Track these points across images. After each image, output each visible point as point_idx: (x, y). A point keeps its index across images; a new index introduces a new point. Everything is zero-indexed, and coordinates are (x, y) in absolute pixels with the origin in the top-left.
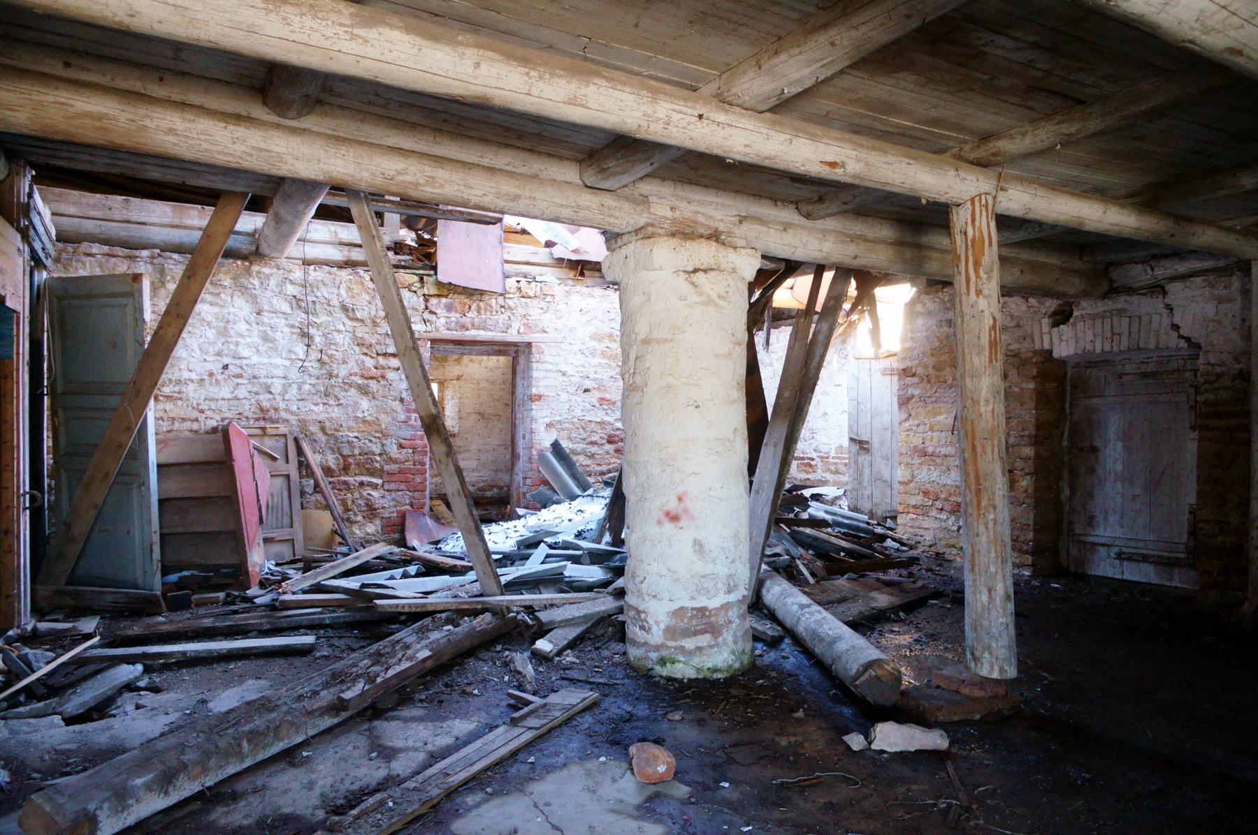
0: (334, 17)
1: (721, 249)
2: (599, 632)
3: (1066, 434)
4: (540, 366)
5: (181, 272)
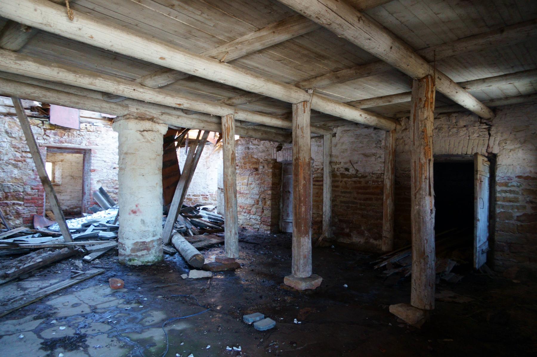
0: (9, 57)
1: (154, 124)
2: (110, 253)
3: (282, 186)
4: (95, 158)
5: (73, 220)
